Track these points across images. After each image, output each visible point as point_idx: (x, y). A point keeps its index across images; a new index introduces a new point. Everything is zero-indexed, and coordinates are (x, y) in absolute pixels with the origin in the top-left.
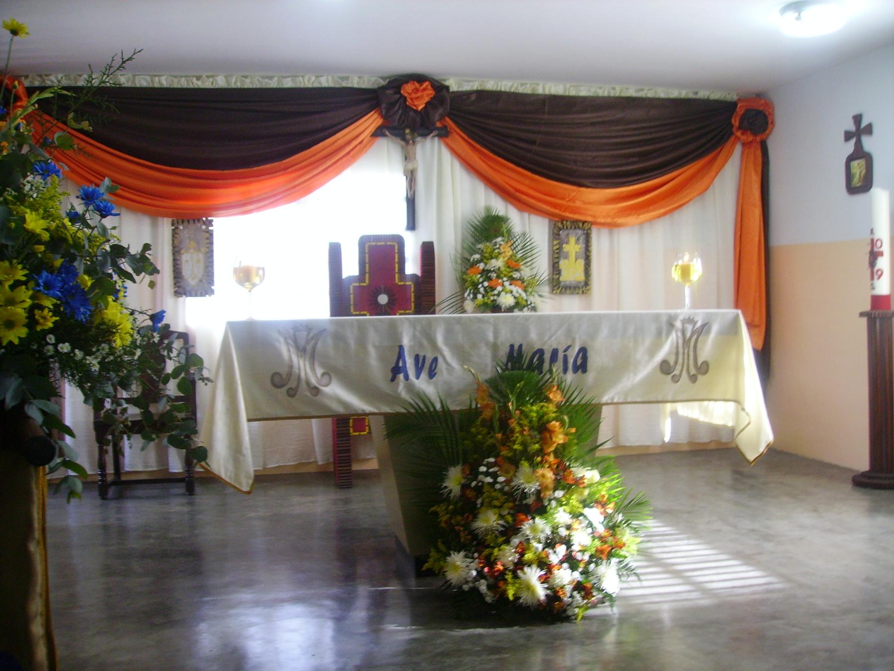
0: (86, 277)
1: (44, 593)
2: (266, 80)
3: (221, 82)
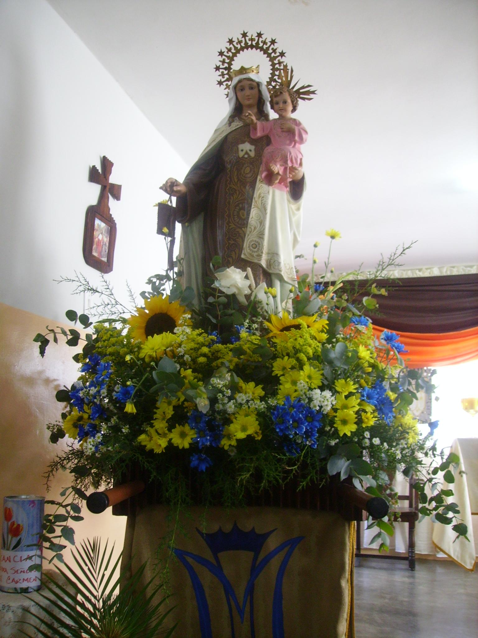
0: (391, 393)
1: (348, 619)
2: (469, 269)
3: (436, 272)
